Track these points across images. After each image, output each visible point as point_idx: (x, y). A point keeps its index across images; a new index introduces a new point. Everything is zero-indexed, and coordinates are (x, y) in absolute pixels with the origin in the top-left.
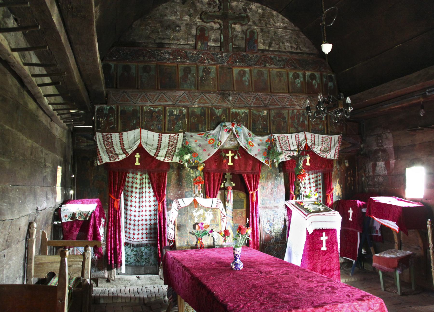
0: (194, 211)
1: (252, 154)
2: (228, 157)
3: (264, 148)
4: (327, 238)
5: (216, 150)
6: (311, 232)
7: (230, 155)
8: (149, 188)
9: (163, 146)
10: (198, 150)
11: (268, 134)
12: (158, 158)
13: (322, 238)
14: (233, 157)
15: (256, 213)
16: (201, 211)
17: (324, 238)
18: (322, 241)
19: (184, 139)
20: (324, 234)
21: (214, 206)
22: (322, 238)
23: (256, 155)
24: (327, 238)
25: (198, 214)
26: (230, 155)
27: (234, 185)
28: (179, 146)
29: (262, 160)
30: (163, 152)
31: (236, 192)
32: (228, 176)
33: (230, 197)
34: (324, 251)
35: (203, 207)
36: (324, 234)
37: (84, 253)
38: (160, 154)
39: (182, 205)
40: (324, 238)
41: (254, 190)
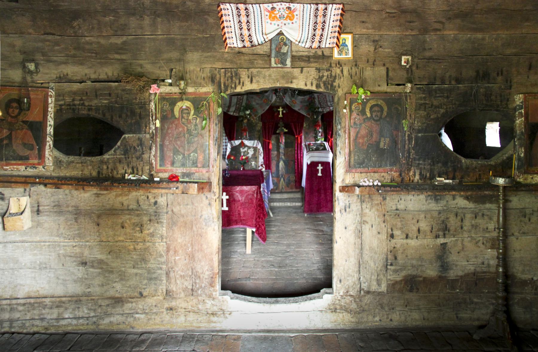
0: (241, 149)
1: (296, 108)
2: (279, 111)
3: (305, 104)
4: (322, 168)
5: (268, 107)
6: (309, 163)
7: (281, 109)
8: (226, 139)
9: (232, 104)
10: (257, 106)
11: (241, 139)
12: (229, 113)
13: (318, 168)
14: (282, 111)
15: (300, 154)
16: (246, 149)
17: (320, 168)
18: (318, 170)
19: (247, 99)
20: (320, 165)
21: (255, 146)
22: (318, 168)
23: (299, 110)
24: (322, 168)
25: (244, 150)
26: (281, 109)
27: (286, 130)
28: (244, 104)
29: (303, 113)
30: (233, 109)
31: (287, 136)
32: (281, 124)
33: (283, 140)
34: (319, 176)
35: (247, 146)
36: (320, 165)
37: (85, 215)
38: (231, 110)
39: (234, 145)
40: (320, 168)
41: (299, 134)
